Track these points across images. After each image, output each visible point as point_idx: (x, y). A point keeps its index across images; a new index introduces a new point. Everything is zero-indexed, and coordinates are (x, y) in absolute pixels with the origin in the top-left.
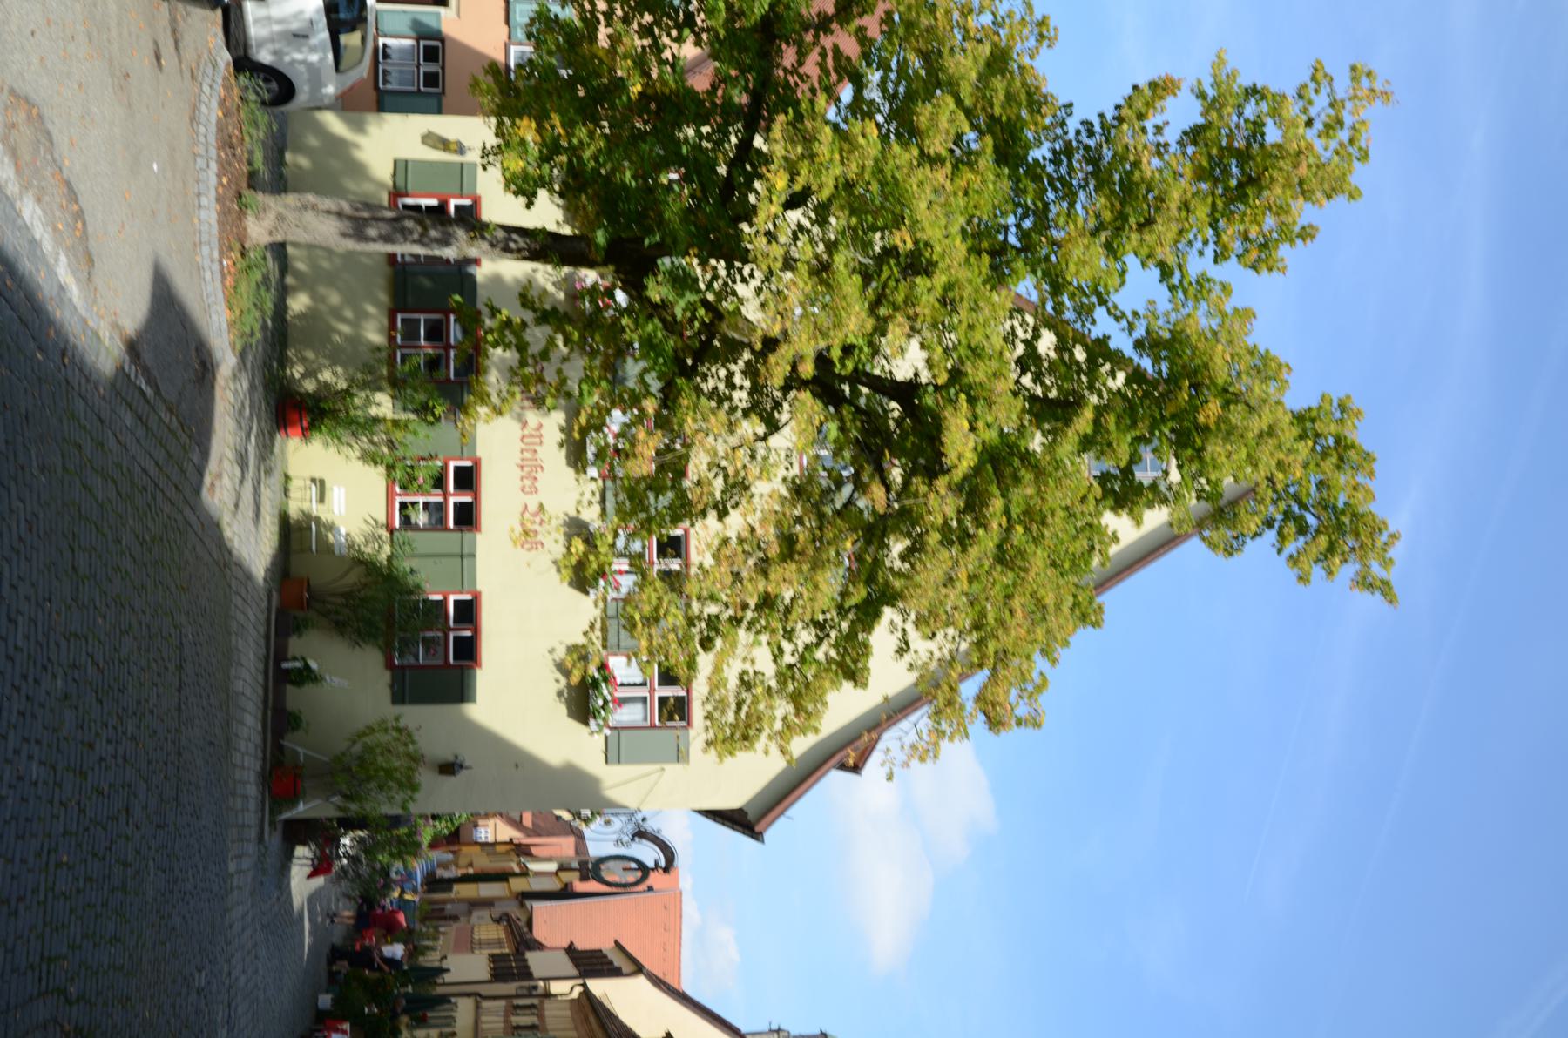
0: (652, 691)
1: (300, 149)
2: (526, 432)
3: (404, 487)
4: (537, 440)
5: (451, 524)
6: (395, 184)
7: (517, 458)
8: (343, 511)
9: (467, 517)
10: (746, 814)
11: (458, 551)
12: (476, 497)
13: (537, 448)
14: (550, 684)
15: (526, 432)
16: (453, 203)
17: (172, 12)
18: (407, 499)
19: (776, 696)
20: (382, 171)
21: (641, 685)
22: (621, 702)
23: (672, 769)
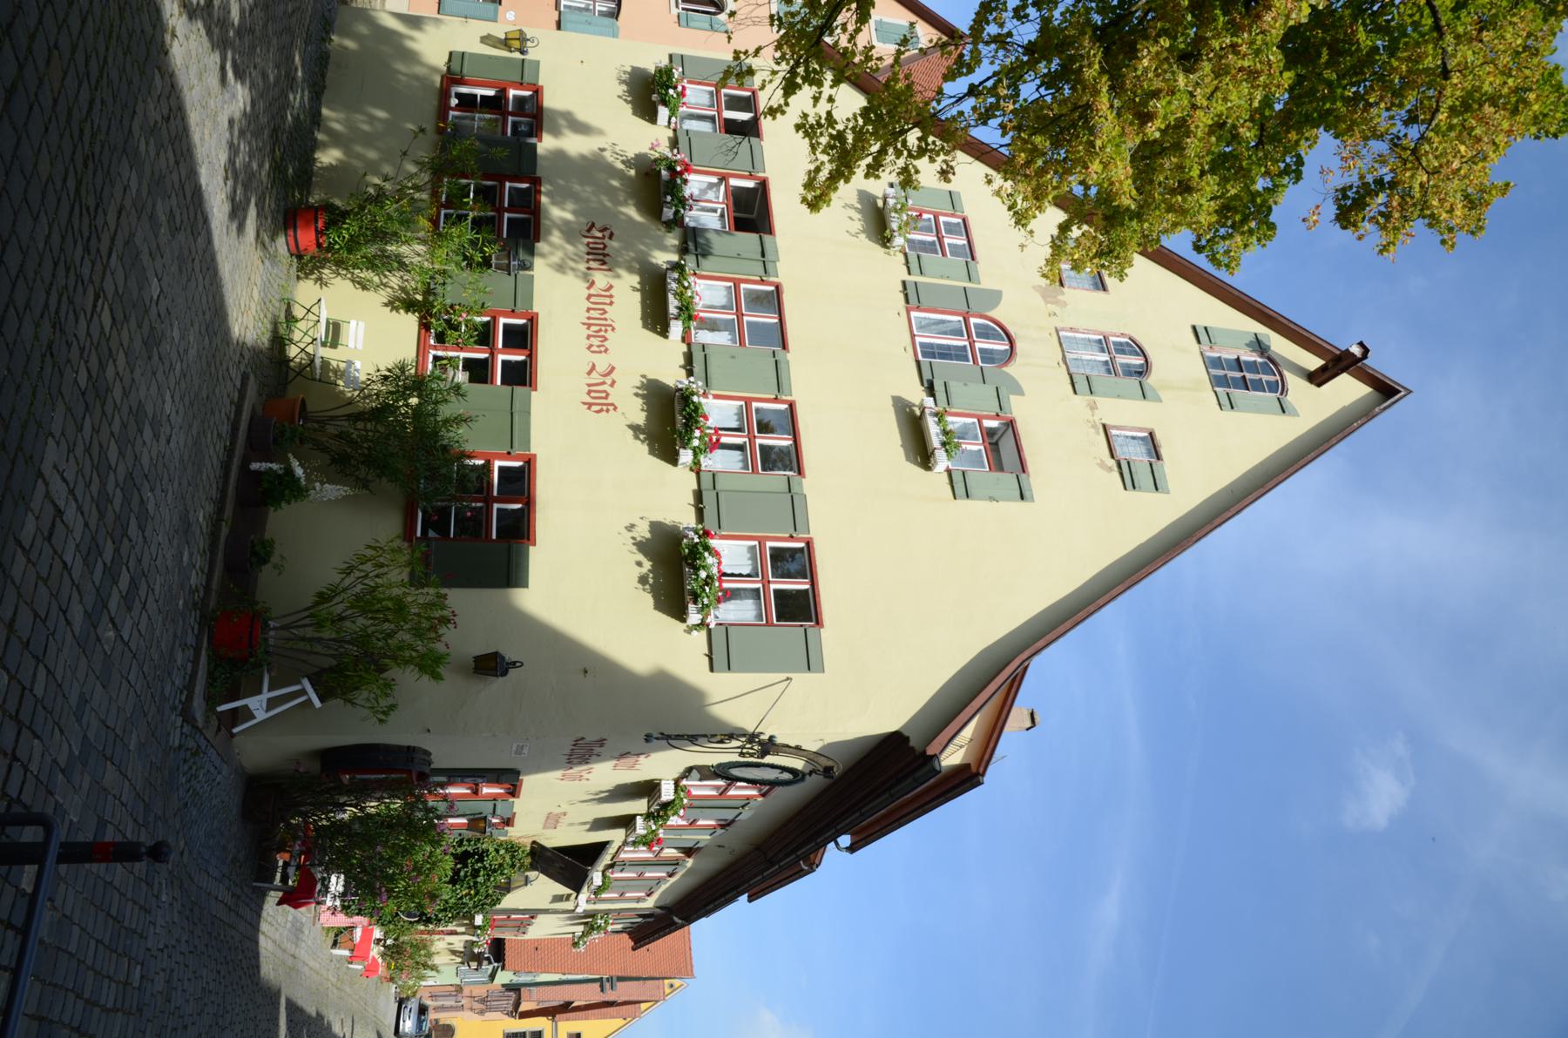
0: (766, 583)
1: (346, 33)
2: (592, 291)
3: (440, 338)
4: (608, 300)
5: (499, 382)
6: (449, 68)
7: (583, 316)
8: (360, 346)
9: (520, 376)
10: (907, 739)
11: (519, 80)
12: (531, 356)
13: (607, 308)
14: (631, 567)
15: (592, 291)
16: (512, 93)
17: (124, 836)
18: (440, 353)
19: (897, 47)
20: (438, 60)
21: (748, 576)
22: (731, 595)
23: (801, 679)
